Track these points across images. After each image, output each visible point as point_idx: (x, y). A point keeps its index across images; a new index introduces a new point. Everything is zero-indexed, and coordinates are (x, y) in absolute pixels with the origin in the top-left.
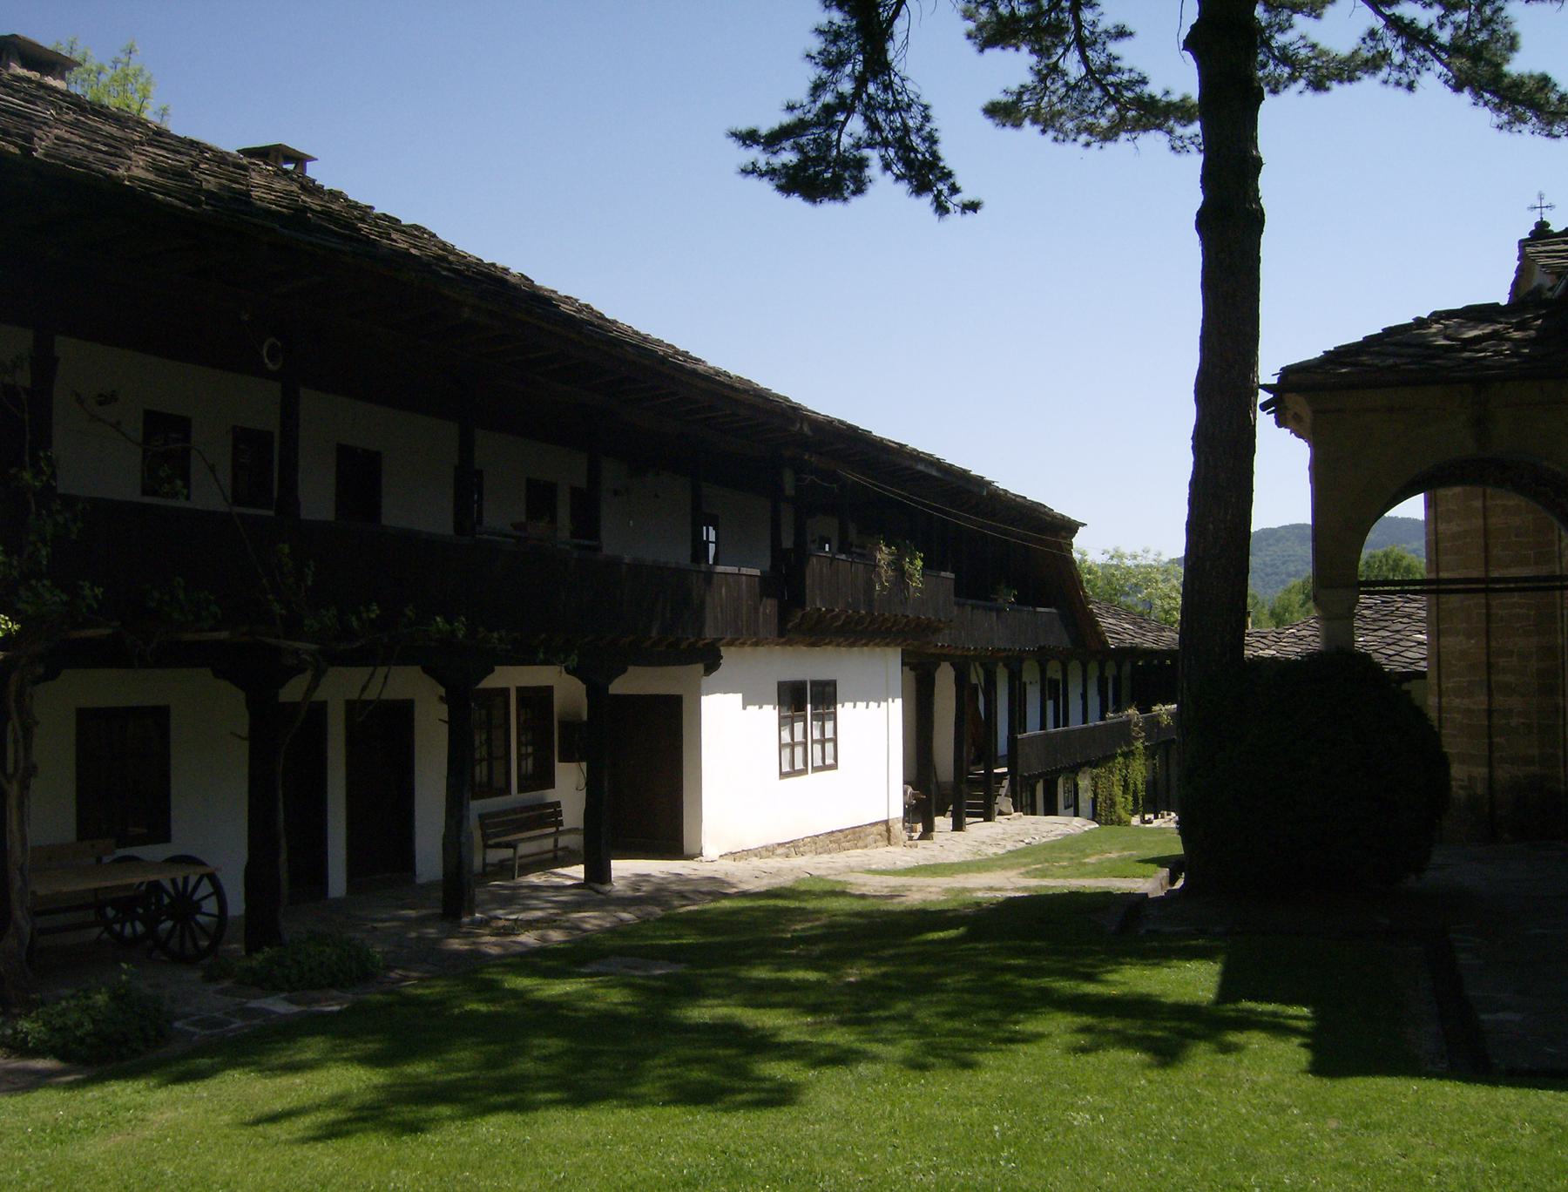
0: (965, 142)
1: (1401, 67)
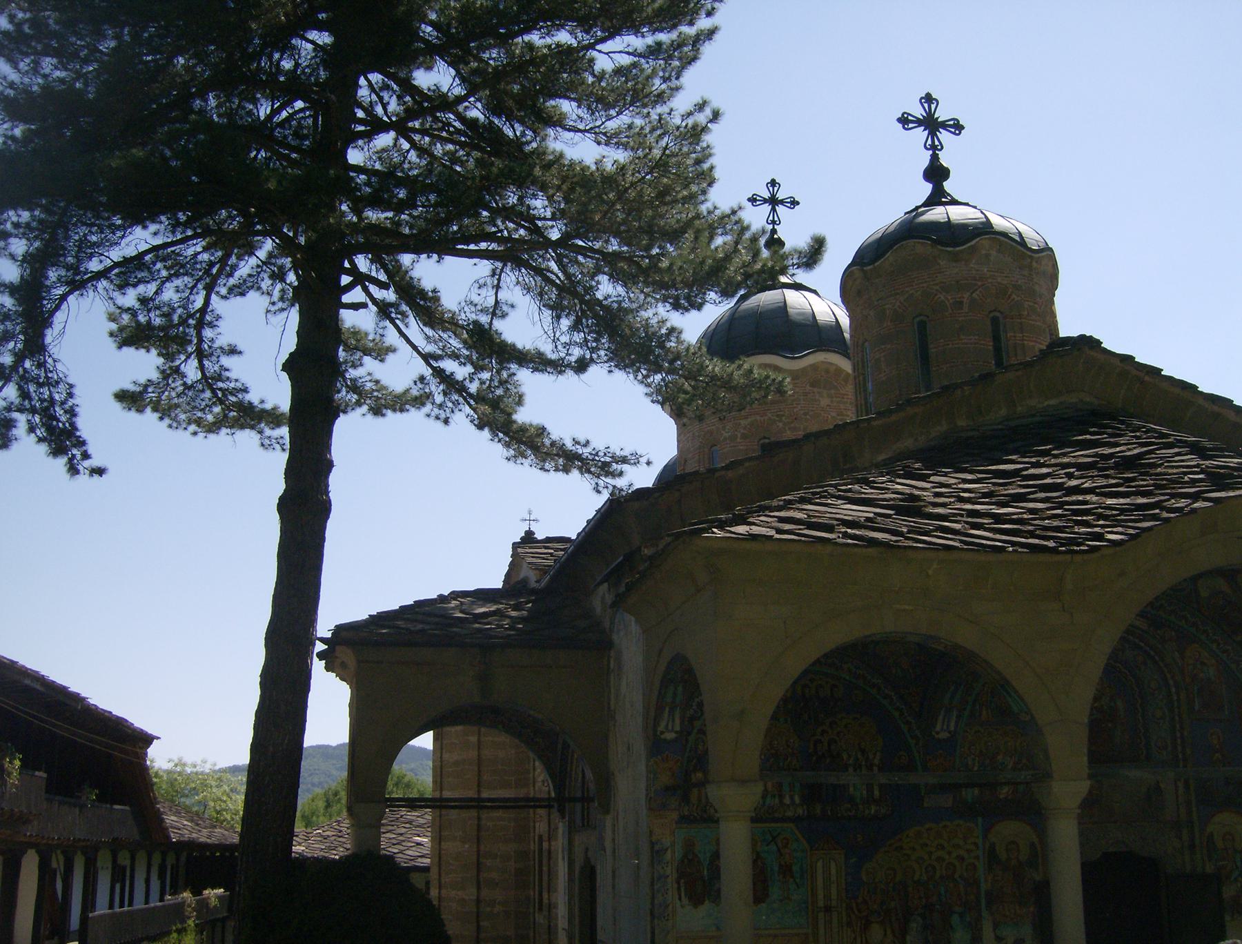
0: (98, 420)
1: (440, 406)
